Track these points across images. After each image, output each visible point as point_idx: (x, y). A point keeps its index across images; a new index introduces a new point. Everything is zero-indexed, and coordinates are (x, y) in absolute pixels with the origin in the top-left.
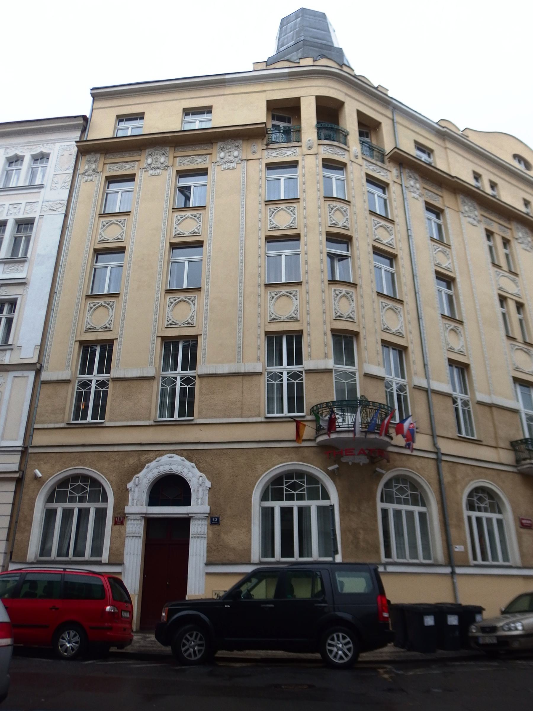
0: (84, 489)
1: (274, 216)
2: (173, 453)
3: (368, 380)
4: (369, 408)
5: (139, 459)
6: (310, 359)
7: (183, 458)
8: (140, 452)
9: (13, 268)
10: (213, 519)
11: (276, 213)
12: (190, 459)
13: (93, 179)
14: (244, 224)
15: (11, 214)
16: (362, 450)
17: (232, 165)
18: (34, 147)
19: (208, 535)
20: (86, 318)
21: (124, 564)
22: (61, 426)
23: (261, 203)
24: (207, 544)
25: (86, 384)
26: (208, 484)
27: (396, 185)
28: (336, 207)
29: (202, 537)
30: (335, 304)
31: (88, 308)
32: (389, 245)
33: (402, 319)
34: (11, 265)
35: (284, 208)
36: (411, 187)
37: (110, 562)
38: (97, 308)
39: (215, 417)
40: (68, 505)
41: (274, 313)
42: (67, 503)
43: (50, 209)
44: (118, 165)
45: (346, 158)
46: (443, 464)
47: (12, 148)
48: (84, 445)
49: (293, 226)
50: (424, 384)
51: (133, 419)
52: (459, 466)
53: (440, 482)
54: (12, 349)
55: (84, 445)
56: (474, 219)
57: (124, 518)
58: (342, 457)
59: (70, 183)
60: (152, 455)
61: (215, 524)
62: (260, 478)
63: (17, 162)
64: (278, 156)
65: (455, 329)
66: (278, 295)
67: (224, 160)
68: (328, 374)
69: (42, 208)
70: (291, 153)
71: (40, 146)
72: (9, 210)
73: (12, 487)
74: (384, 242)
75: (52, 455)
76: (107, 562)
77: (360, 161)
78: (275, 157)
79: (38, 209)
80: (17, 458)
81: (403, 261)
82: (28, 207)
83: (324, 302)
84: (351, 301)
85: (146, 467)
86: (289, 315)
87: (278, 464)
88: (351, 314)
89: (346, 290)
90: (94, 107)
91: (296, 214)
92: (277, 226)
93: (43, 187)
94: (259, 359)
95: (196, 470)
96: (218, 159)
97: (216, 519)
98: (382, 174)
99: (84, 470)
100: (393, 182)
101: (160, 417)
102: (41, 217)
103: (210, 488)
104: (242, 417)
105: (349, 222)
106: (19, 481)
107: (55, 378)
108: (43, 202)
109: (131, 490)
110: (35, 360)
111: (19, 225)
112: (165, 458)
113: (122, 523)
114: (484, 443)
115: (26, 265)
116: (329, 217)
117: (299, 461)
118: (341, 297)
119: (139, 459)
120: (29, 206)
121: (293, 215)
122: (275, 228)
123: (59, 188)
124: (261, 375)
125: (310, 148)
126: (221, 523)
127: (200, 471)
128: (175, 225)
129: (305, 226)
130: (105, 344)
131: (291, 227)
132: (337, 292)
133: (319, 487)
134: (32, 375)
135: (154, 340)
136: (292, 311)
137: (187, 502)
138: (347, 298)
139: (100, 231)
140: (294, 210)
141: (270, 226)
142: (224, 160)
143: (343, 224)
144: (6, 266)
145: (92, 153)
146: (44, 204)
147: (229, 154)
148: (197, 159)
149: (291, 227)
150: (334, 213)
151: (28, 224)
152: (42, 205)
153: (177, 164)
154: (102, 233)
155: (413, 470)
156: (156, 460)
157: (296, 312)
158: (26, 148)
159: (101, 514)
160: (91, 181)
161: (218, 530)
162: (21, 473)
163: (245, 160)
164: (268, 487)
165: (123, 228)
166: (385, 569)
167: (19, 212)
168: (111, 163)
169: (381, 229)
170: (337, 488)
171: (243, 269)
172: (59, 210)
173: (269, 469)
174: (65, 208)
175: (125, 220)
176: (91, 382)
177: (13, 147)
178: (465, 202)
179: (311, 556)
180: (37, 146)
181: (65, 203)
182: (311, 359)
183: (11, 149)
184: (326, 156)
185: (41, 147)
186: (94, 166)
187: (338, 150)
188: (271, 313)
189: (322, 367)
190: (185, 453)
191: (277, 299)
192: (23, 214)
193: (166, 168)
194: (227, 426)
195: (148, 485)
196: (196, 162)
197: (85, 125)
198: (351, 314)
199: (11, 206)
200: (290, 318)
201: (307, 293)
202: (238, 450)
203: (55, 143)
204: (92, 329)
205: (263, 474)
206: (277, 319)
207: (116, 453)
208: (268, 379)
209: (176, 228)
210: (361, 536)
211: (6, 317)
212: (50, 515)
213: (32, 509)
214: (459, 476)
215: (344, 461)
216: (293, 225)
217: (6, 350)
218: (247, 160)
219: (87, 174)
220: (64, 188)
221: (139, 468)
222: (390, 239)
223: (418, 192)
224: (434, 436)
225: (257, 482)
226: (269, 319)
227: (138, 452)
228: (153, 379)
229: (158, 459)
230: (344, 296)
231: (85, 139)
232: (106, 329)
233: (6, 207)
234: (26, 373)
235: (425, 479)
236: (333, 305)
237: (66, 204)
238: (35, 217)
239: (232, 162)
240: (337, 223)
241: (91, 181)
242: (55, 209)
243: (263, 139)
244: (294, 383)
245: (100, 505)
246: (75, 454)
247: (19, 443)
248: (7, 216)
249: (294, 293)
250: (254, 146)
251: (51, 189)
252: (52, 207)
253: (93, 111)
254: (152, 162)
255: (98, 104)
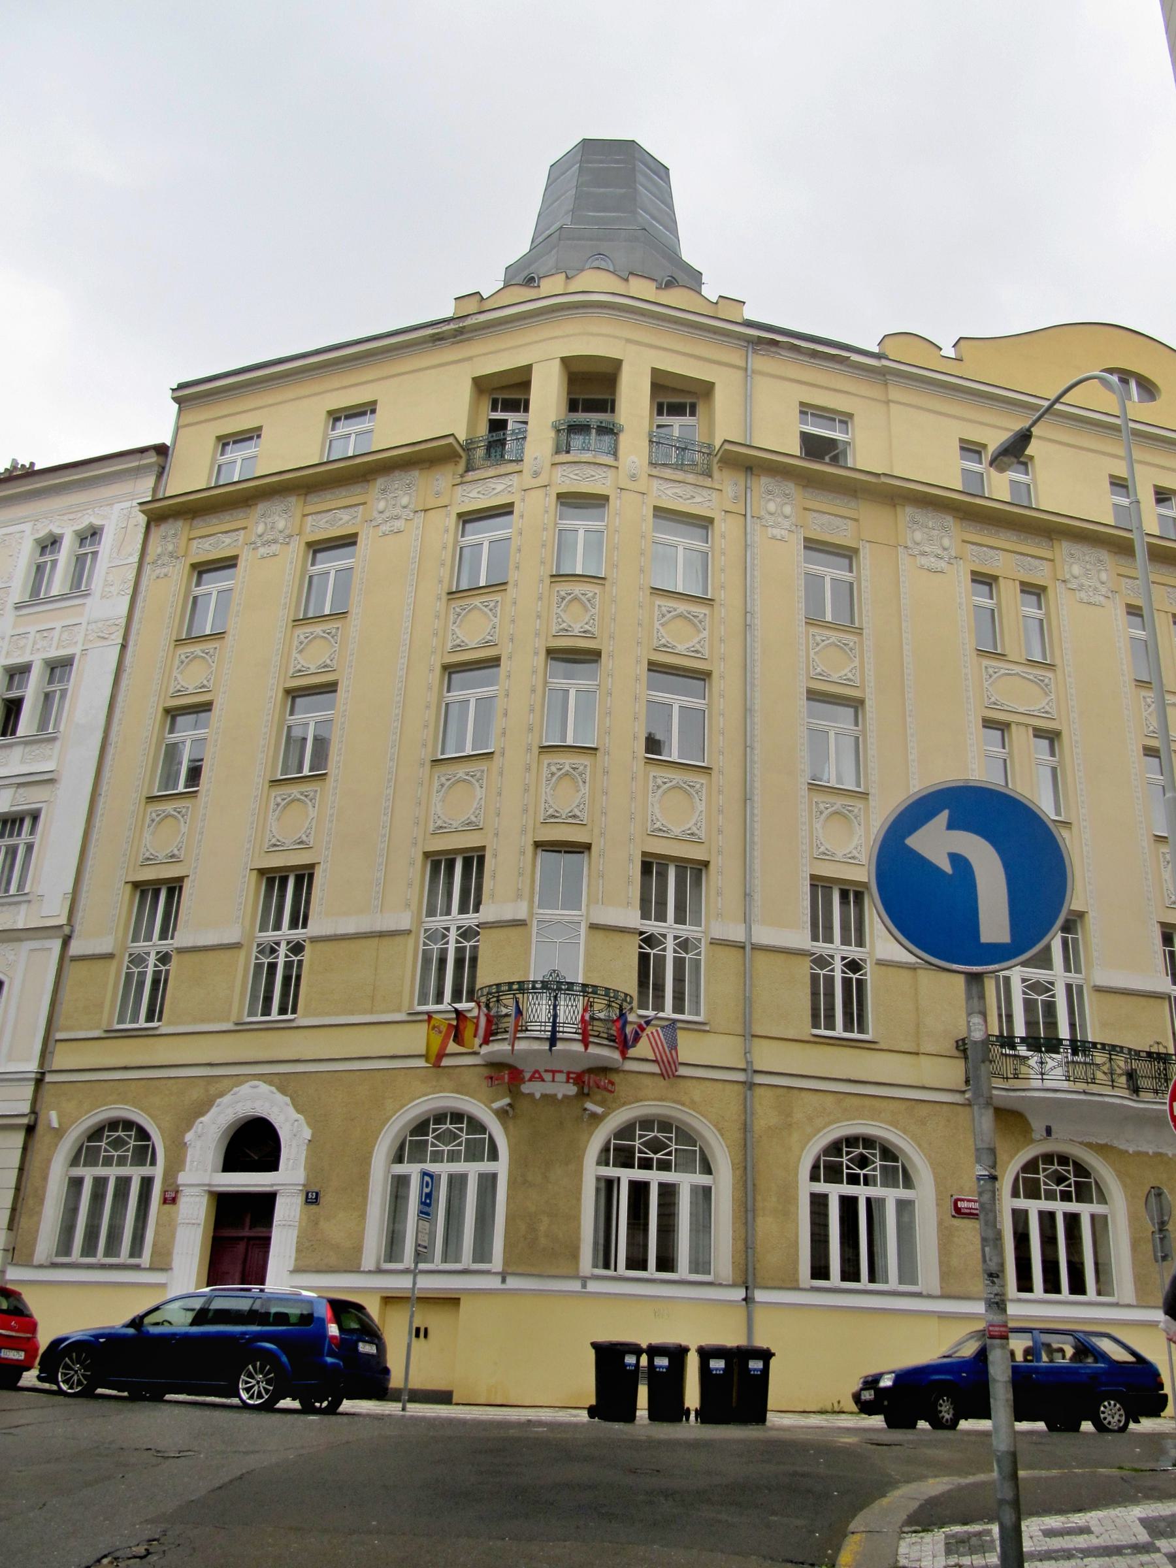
0: (126, 1143)
1: (461, 621)
2: (259, 1080)
3: (600, 935)
4: (565, 994)
5: (207, 1091)
6: (491, 901)
7: (273, 1089)
8: (209, 1078)
9: (38, 752)
10: (310, 1194)
11: (464, 616)
12: (283, 1090)
13: (169, 572)
14: (408, 642)
15: (39, 649)
16: (536, 1071)
17: (399, 524)
18: (80, 515)
19: (300, 1222)
20: (1164, 882)
21: (171, 1269)
22: (96, 1036)
23: (440, 599)
24: (298, 1237)
25: (138, 960)
26: (307, 1133)
27: (729, 517)
28: (570, 594)
29: (290, 1225)
30: (546, 793)
31: (148, 821)
32: (692, 654)
33: (701, 806)
34: (35, 747)
35: (479, 605)
36: (767, 516)
37: (152, 1266)
38: (162, 820)
39: (328, 1014)
40: (100, 1171)
41: (442, 816)
42: (99, 1168)
43: (99, 637)
44: (212, 540)
45: (608, 484)
46: (759, 1091)
47: (44, 520)
48: (125, 1068)
49: (492, 641)
50: (736, 933)
51: (203, 1021)
52: (803, 1094)
53: (746, 1128)
54: (29, 901)
55: (125, 1068)
56: (937, 556)
57: (177, 1192)
58: (524, 1083)
59: (132, 583)
60: (226, 1082)
61: (312, 1203)
62: (388, 1122)
63: (54, 546)
64: (481, 496)
65: (844, 811)
66: (667, 785)
67: (387, 514)
68: (520, 929)
69: (86, 635)
70: (503, 486)
71: (88, 511)
72: (35, 643)
73: (18, 1138)
74: (681, 648)
75: (79, 1084)
76: (148, 1266)
77: (642, 484)
78: (476, 497)
79: (80, 638)
80: (28, 1090)
81: (726, 682)
82: (65, 636)
83: (526, 790)
84: (581, 783)
85: (216, 1104)
86: (466, 818)
87: (420, 1097)
88: (576, 810)
89: (571, 761)
90: (181, 424)
91: (498, 615)
92: (463, 642)
93: (89, 594)
94: (408, 905)
95: (291, 1110)
96: (375, 514)
97: (314, 1194)
98: (698, 499)
99: (123, 1110)
100: (723, 513)
101: (249, 1016)
102: (84, 652)
103: (310, 1141)
104: (372, 1013)
105: (596, 623)
106: (30, 1130)
107: (89, 952)
108: (88, 623)
109: (190, 1144)
110: (63, 920)
111: (52, 669)
112: (245, 1089)
113: (174, 1201)
114: (882, 1046)
115: (58, 744)
116: (555, 616)
117: (453, 1092)
118: (560, 778)
119: (207, 1091)
120: (66, 633)
121: (493, 618)
122: (460, 646)
123: (115, 594)
124: (408, 934)
125: (536, 474)
126: (322, 1200)
127: (298, 1111)
128: (294, 654)
129: (512, 640)
130: (174, 885)
131: (487, 642)
132: (554, 769)
133: (485, 1138)
134: (57, 944)
135: (245, 876)
136: (471, 812)
137: (271, 1165)
138: (573, 779)
139: (175, 673)
140: (495, 607)
141: (451, 645)
142: (387, 514)
143: (582, 628)
144: (28, 749)
145: (171, 521)
146: (90, 627)
147: (394, 502)
148: (341, 516)
149: (487, 642)
150: (567, 606)
151: (67, 666)
152: (87, 630)
153: (308, 529)
154: (179, 676)
155: (683, 1104)
156: (232, 1092)
157: (478, 812)
158: (66, 518)
159: (147, 1183)
160: (166, 575)
161: (316, 1213)
162: (33, 1117)
163: (421, 511)
164: (406, 1137)
165: (212, 664)
166: (584, 1286)
167: (50, 647)
168: (200, 537)
169: (680, 623)
170: (508, 1141)
171: (398, 734)
172: (113, 637)
173: (405, 1106)
174: (122, 632)
175: (216, 648)
176: (148, 954)
177: (46, 518)
178: (916, 523)
179: (887, 1282)
180: (85, 512)
181: (123, 622)
182: (493, 903)
183: (43, 522)
184: (564, 489)
185: (90, 515)
186: (170, 548)
187: (590, 470)
188: (436, 817)
189: (508, 916)
190: (276, 1080)
191: (450, 787)
192: (57, 649)
193: (287, 540)
194: (347, 1029)
195: (217, 1136)
196: (341, 522)
197: (162, 464)
198: (576, 810)
199: (38, 635)
200: (467, 824)
201: (501, 774)
202: (358, 1073)
203: (113, 504)
204: (151, 859)
205: (394, 1115)
206: (445, 828)
207: (172, 1081)
208: (424, 942)
209: (296, 659)
210: (543, 1228)
211: (25, 843)
212: (76, 1184)
213: (45, 1178)
214: (798, 1116)
215: (526, 1091)
216: (491, 638)
217: (19, 903)
218: (426, 511)
219: (159, 562)
220: (123, 593)
221: (202, 1108)
222: (697, 639)
223: (786, 524)
224: (749, 1036)
225: (382, 1130)
226: (431, 828)
227: (206, 1079)
228: (240, 948)
229: (236, 1089)
230: (567, 774)
231: (161, 496)
232: (174, 859)
233: (31, 636)
234: (47, 943)
235: (710, 1122)
236: (544, 793)
237: (124, 624)
238: (75, 654)
239: (398, 518)
240: (570, 626)
241: (166, 575)
242: (107, 636)
243: (456, 463)
244: (466, 946)
245: (486, 1166)
246: (112, 1084)
247: (33, 1066)
248: (32, 654)
249: (478, 774)
250: (437, 480)
251: (102, 597)
252: (102, 632)
253: (180, 431)
254: (265, 530)
255: (189, 418)
